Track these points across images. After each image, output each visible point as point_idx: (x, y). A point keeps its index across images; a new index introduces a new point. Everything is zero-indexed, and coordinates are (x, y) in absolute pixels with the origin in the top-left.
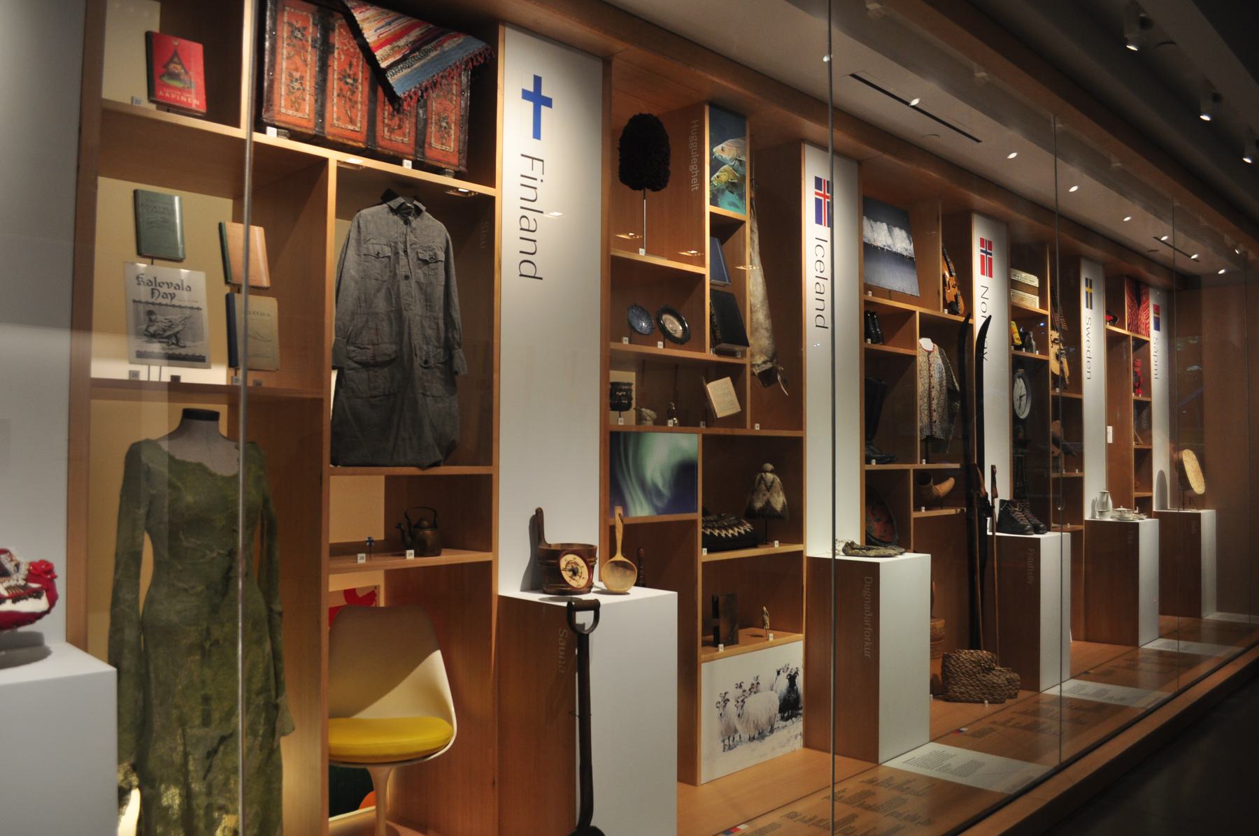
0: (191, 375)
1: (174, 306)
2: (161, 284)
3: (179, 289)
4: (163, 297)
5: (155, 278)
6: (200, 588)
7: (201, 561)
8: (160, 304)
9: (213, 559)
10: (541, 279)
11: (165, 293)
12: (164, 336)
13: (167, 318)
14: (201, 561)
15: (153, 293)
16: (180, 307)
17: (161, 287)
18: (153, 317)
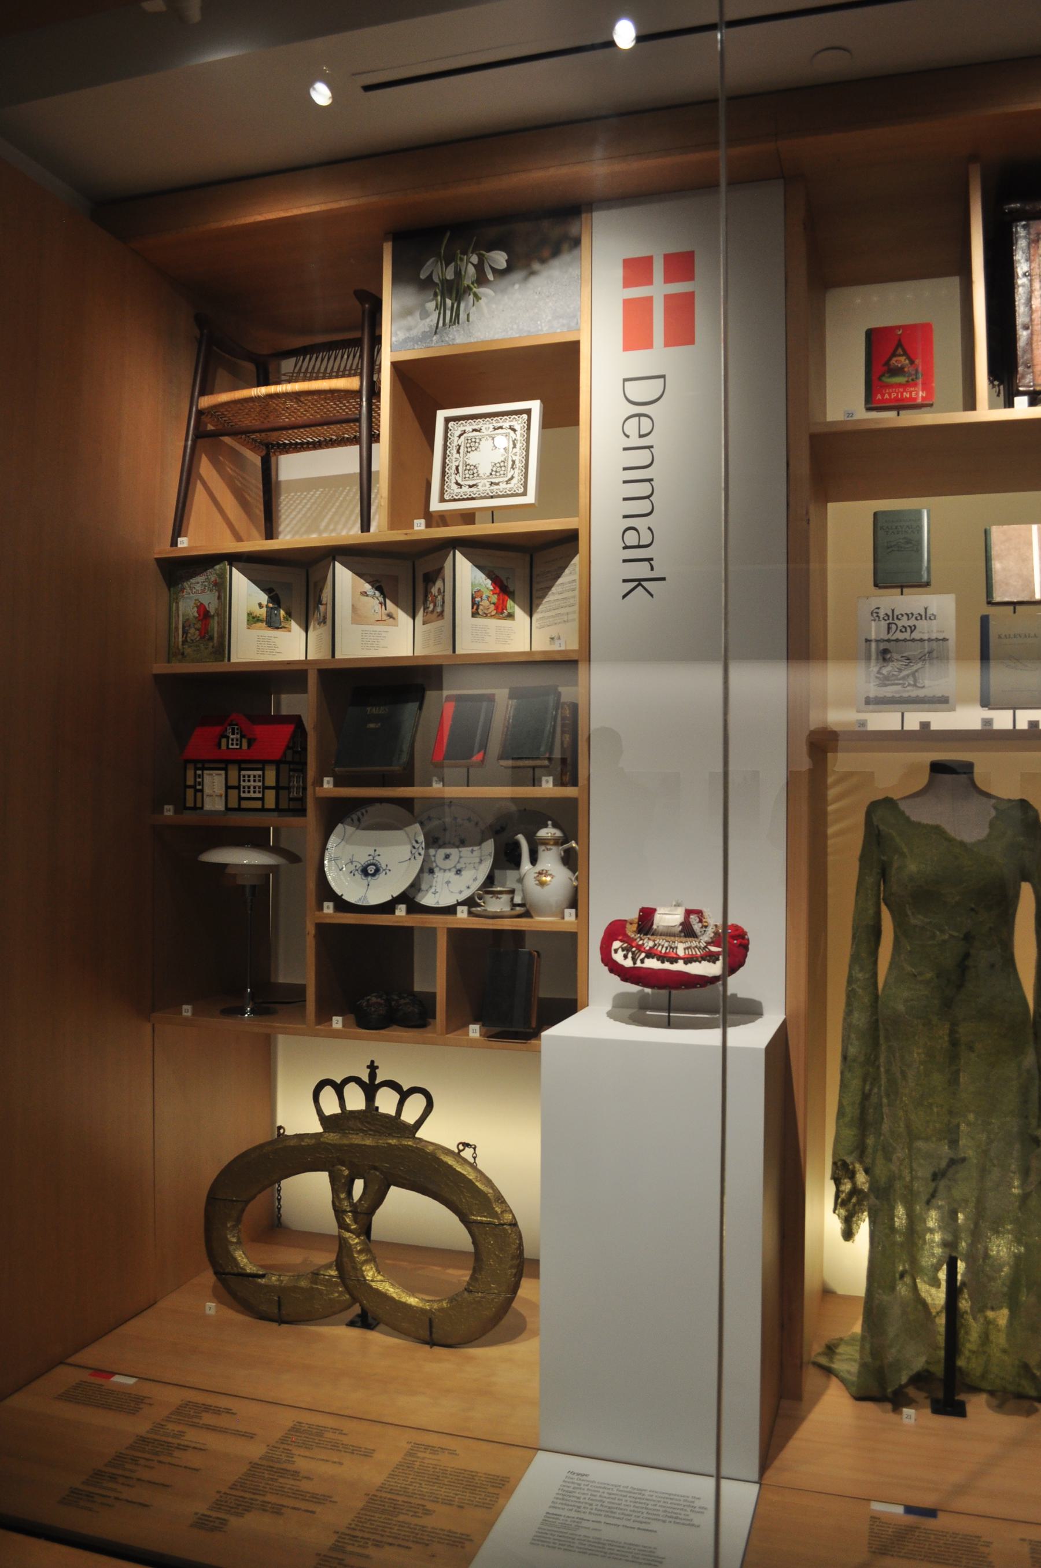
0: (941, 721)
1: (913, 640)
2: (900, 617)
3: (921, 619)
4: (901, 631)
5: (893, 611)
6: (929, 975)
7: (930, 942)
8: (897, 640)
9: (944, 942)
10: (664, 579)
11: (904, 626)
12: (899, 677)
13: (904, 655)
14: (930, 942)
15: (889, 628)
16: (922, 640)
17: (899, 620)
18: (888, 656)
